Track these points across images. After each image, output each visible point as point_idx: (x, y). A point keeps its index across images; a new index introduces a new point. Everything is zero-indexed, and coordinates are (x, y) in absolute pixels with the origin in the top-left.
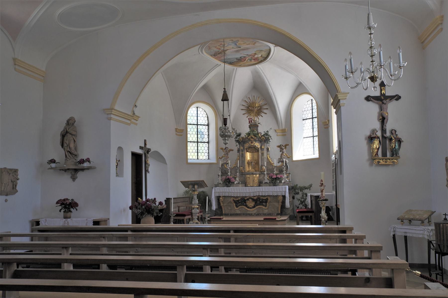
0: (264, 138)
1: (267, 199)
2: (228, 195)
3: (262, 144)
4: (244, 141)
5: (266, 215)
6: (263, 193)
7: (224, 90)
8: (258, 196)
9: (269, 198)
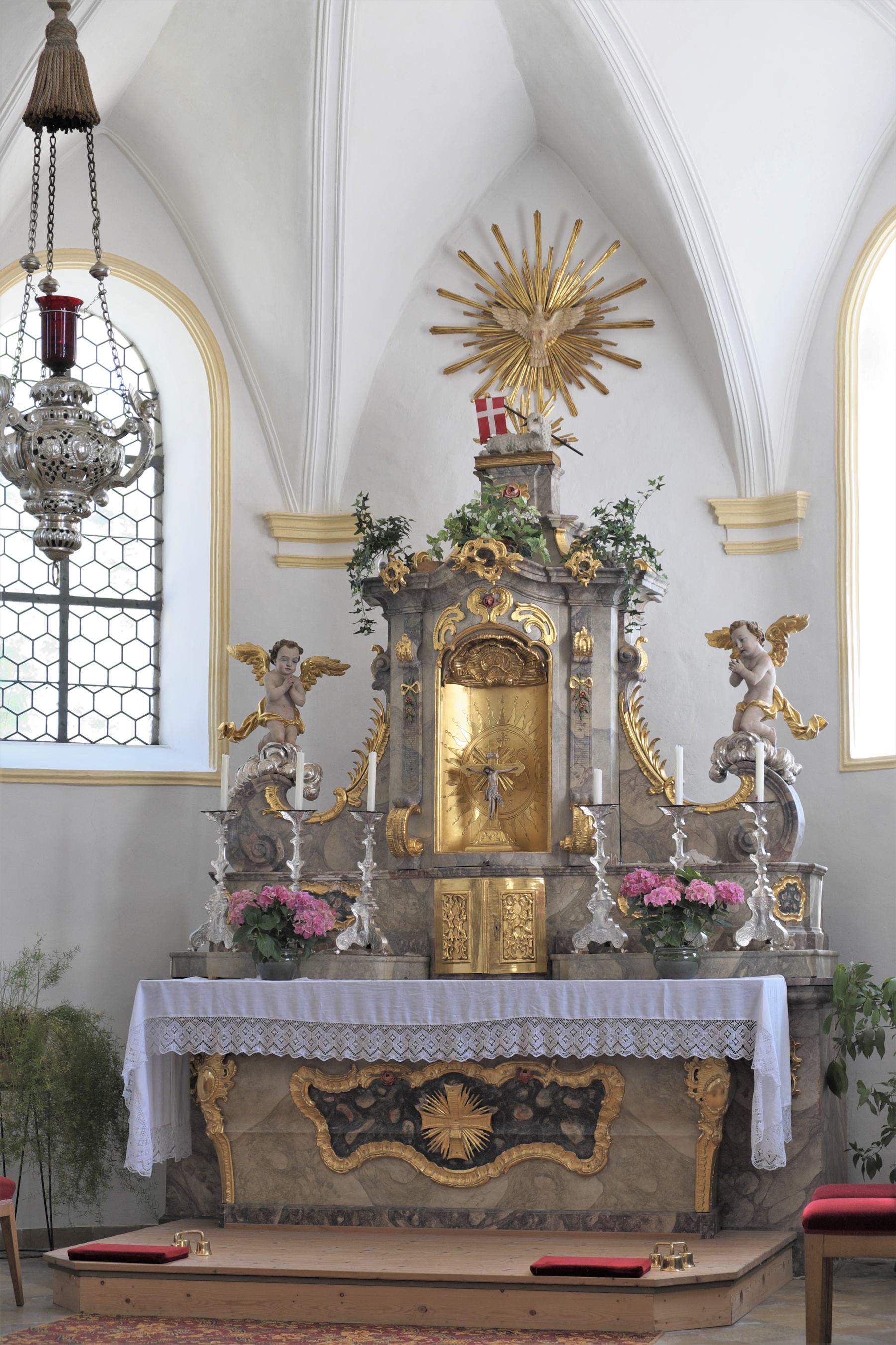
0: (592, 563)
1: (597, 1085)
2: (259, 1049)
3: (582, 613)
4: (427, 591)
5: (587, 1229)
6: (486, 1043)
7: (51, 15)
8: (516, 1058)
9: (612, 1080)
